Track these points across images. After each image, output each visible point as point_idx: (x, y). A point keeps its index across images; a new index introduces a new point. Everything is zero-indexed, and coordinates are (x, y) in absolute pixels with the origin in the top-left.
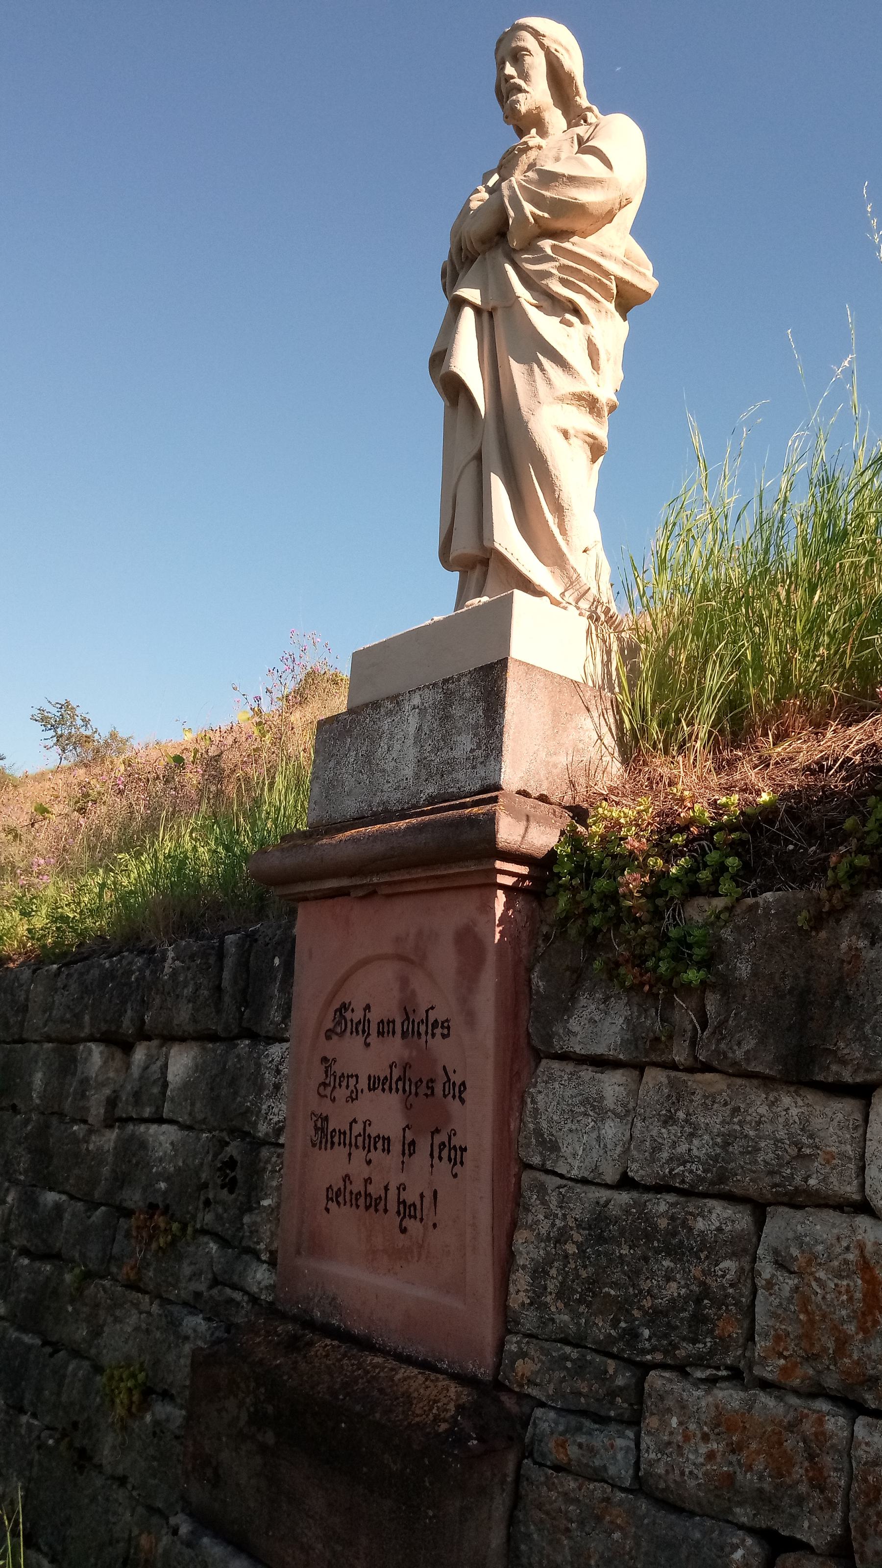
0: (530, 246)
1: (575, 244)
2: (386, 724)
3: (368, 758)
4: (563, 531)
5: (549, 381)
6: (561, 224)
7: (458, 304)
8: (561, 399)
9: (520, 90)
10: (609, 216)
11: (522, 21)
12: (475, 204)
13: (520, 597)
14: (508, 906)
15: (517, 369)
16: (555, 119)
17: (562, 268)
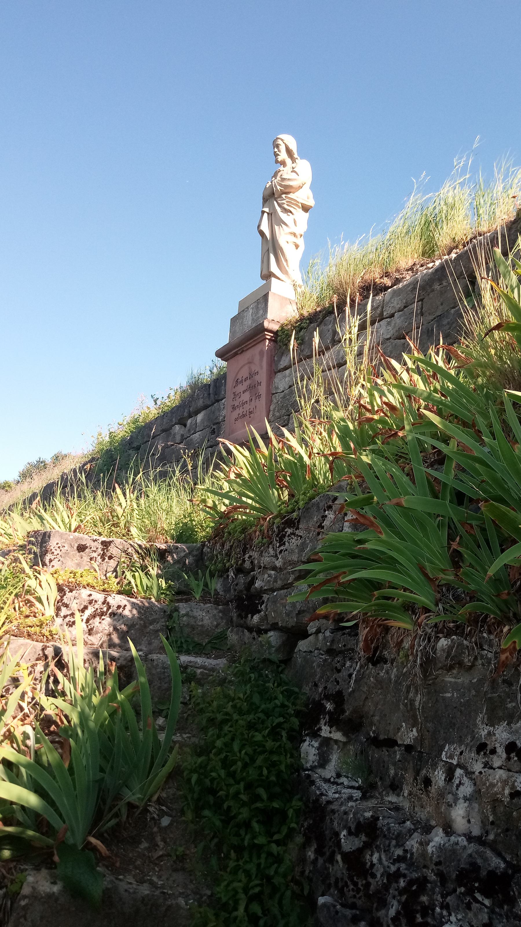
0: (280, 196)
1: (291, 196)
2: (245, 314)
3: (242, 322)
4: (288, 266)
5: (283, 230)
6: (287, 191)
7: (263, 212)
8: (286, 234)
9: (279, 155)
10: (300, 187)
11: (278, 137)
12: (267, 186)
13: (273, 279)
14: (269, 343)
15: (276, 227)
16: (288, 161)
17: (287, 202)
